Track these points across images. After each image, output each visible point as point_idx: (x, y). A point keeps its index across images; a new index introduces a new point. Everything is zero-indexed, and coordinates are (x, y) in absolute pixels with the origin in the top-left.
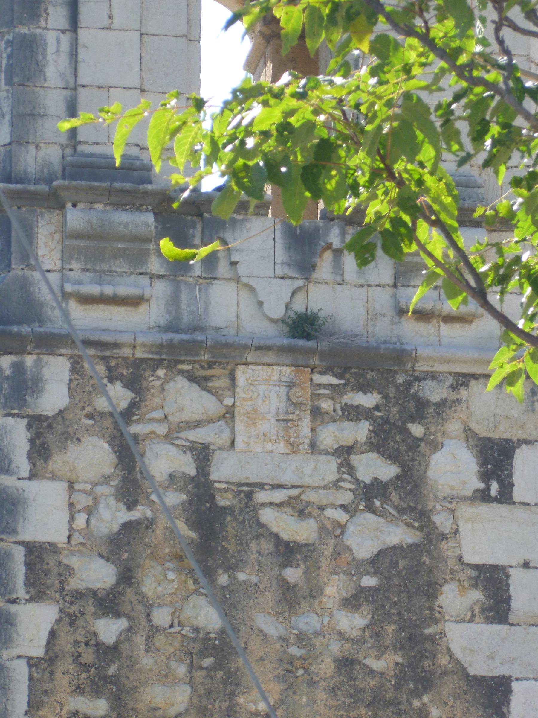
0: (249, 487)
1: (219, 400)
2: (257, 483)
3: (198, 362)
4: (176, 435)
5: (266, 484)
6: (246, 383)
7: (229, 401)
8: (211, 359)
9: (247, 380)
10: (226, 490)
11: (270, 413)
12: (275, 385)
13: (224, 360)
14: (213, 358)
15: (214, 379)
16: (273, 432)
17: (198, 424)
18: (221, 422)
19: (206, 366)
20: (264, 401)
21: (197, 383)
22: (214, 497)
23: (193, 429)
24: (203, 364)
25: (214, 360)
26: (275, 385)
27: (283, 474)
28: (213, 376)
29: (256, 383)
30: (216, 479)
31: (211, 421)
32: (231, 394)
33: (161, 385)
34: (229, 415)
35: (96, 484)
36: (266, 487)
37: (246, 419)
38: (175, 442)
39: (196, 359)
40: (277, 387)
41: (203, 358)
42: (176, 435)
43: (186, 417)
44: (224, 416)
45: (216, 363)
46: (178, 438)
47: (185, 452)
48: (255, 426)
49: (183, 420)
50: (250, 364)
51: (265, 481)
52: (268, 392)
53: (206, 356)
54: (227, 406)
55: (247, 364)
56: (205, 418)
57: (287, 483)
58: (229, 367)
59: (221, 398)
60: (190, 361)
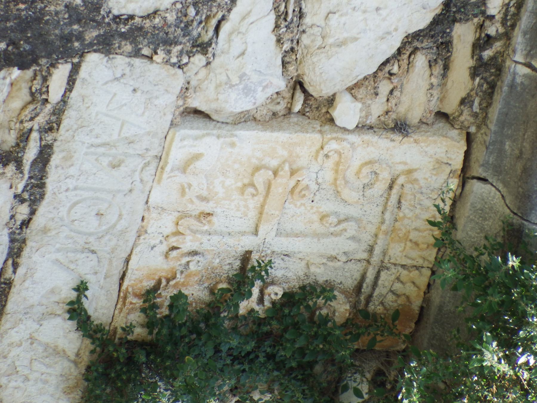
0: (34, 163)
1: (357, 85)
2: (42, 186)
3: (507, 36)
5: (33, 212)
7: (347, 112)
8: (507, 79)
9: (410, 172)
10: (37, 97)
11: (279, 234)
12: (371, 250)
13: (495, 112)
14: (512, 86)
15: (438, 70)
18: (280, 84)
19: (487, 54)
22: (22, 67)
24: (498, 46)
25: (503, 88)
26: (371, 250)
27: (57, 261)
28: (446, 68)
30: (83, 72)
32: (372, 120)
35: (100, 156)
36: (23, 210)
39: (519, 39)
40: (365, 256)
41: (519, 57)
44: (299, 84)
45: (493, 87)
50: (463, 184)
51: (43, 209)
52: (351, 232)
53: (523, 70)
55: (465, 175)
56: (305, 40)
57: (21, 271)
58: (466, 117)
60: (517, 16)
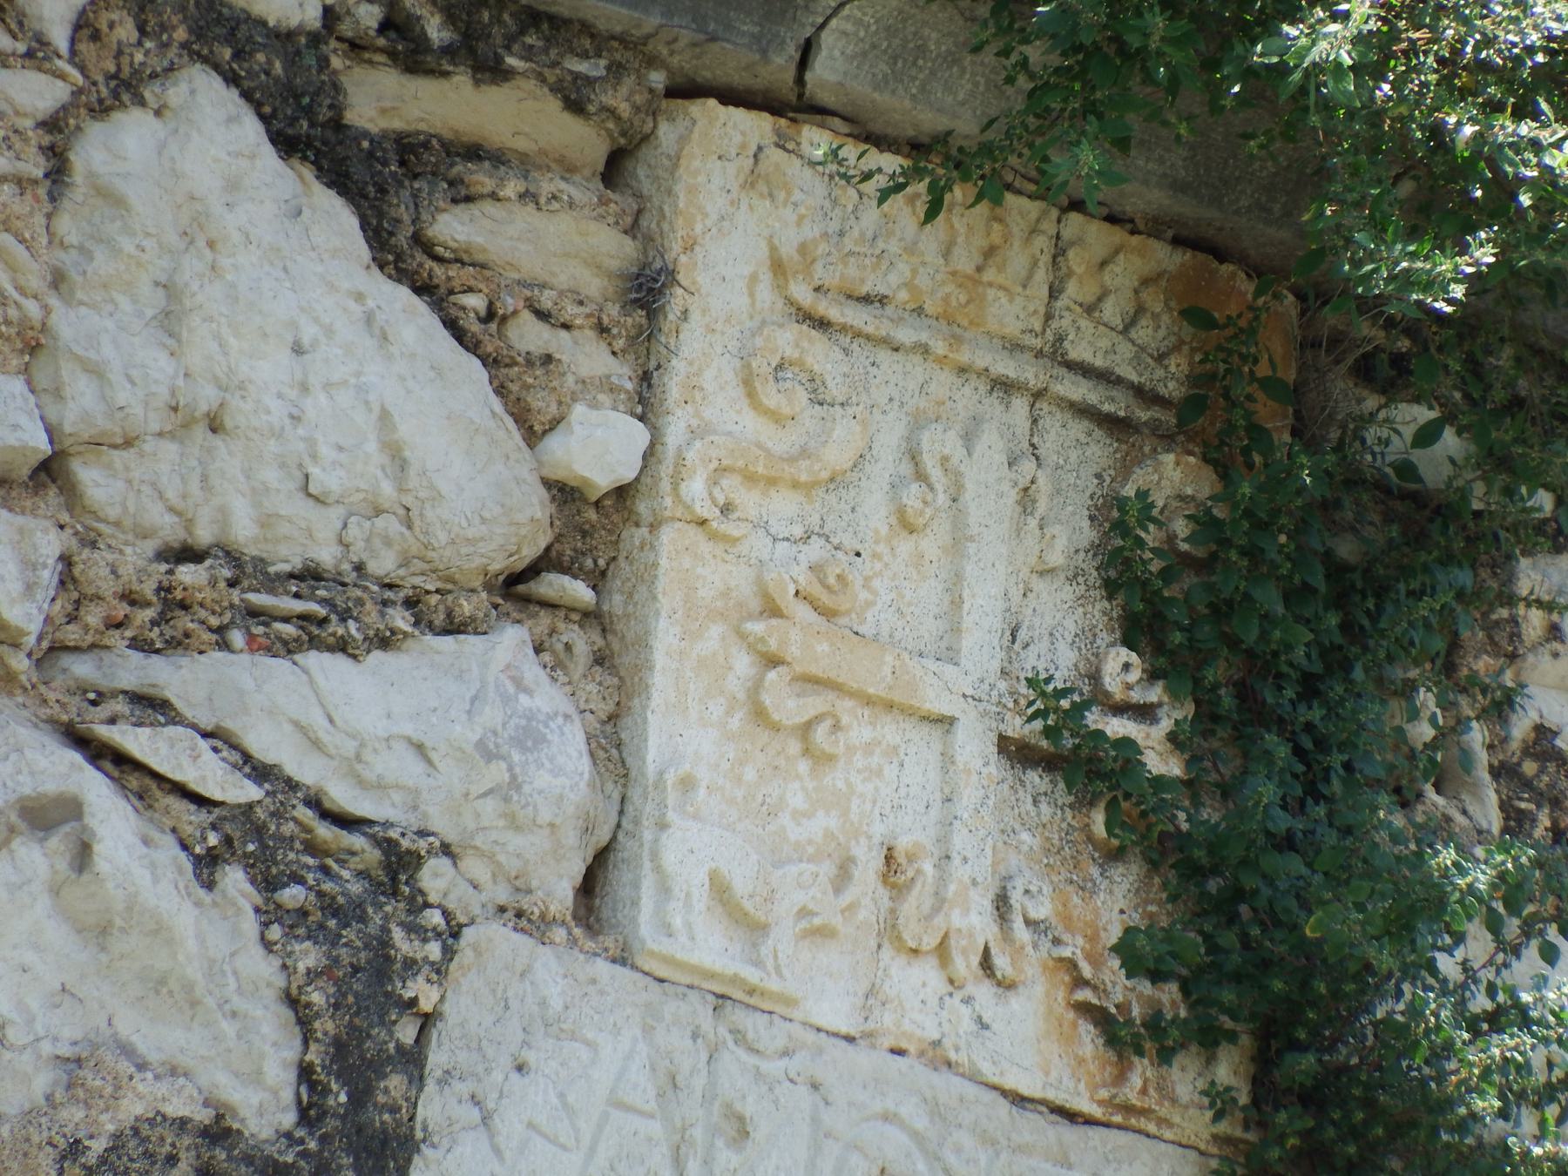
4: (131, 670)
6: (766, 293)
7: (599, 446)
9: (778, 267)
11: (950, 655)
15: (481, 178)
16: (974, 862)
17: (323, 610)
18: (510, 641)
20: (906, 524)
21: (338, 179)
23: (289, 649)
26: (1004, 387)
28: (474, 152)
29: (856, 316)
31: (434, 613)
32: (623, 374)
33: (52, 124)
34: (571, 575)
37: (743, 664)
38: (136, 741)
40: (1020, 405)
42: (131, 670)
43: (244, 504)
46: (152, 706)
47: (207, 865)
48: (821, 760)
49: (204, 536)
52: (952, 444)
54: (564, 493)
55: (792, 105)
56: (383, 564)
59: (541, 404)
